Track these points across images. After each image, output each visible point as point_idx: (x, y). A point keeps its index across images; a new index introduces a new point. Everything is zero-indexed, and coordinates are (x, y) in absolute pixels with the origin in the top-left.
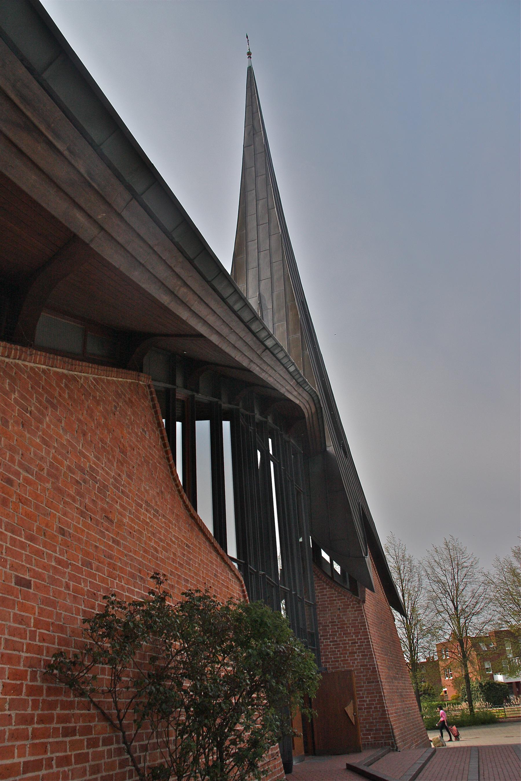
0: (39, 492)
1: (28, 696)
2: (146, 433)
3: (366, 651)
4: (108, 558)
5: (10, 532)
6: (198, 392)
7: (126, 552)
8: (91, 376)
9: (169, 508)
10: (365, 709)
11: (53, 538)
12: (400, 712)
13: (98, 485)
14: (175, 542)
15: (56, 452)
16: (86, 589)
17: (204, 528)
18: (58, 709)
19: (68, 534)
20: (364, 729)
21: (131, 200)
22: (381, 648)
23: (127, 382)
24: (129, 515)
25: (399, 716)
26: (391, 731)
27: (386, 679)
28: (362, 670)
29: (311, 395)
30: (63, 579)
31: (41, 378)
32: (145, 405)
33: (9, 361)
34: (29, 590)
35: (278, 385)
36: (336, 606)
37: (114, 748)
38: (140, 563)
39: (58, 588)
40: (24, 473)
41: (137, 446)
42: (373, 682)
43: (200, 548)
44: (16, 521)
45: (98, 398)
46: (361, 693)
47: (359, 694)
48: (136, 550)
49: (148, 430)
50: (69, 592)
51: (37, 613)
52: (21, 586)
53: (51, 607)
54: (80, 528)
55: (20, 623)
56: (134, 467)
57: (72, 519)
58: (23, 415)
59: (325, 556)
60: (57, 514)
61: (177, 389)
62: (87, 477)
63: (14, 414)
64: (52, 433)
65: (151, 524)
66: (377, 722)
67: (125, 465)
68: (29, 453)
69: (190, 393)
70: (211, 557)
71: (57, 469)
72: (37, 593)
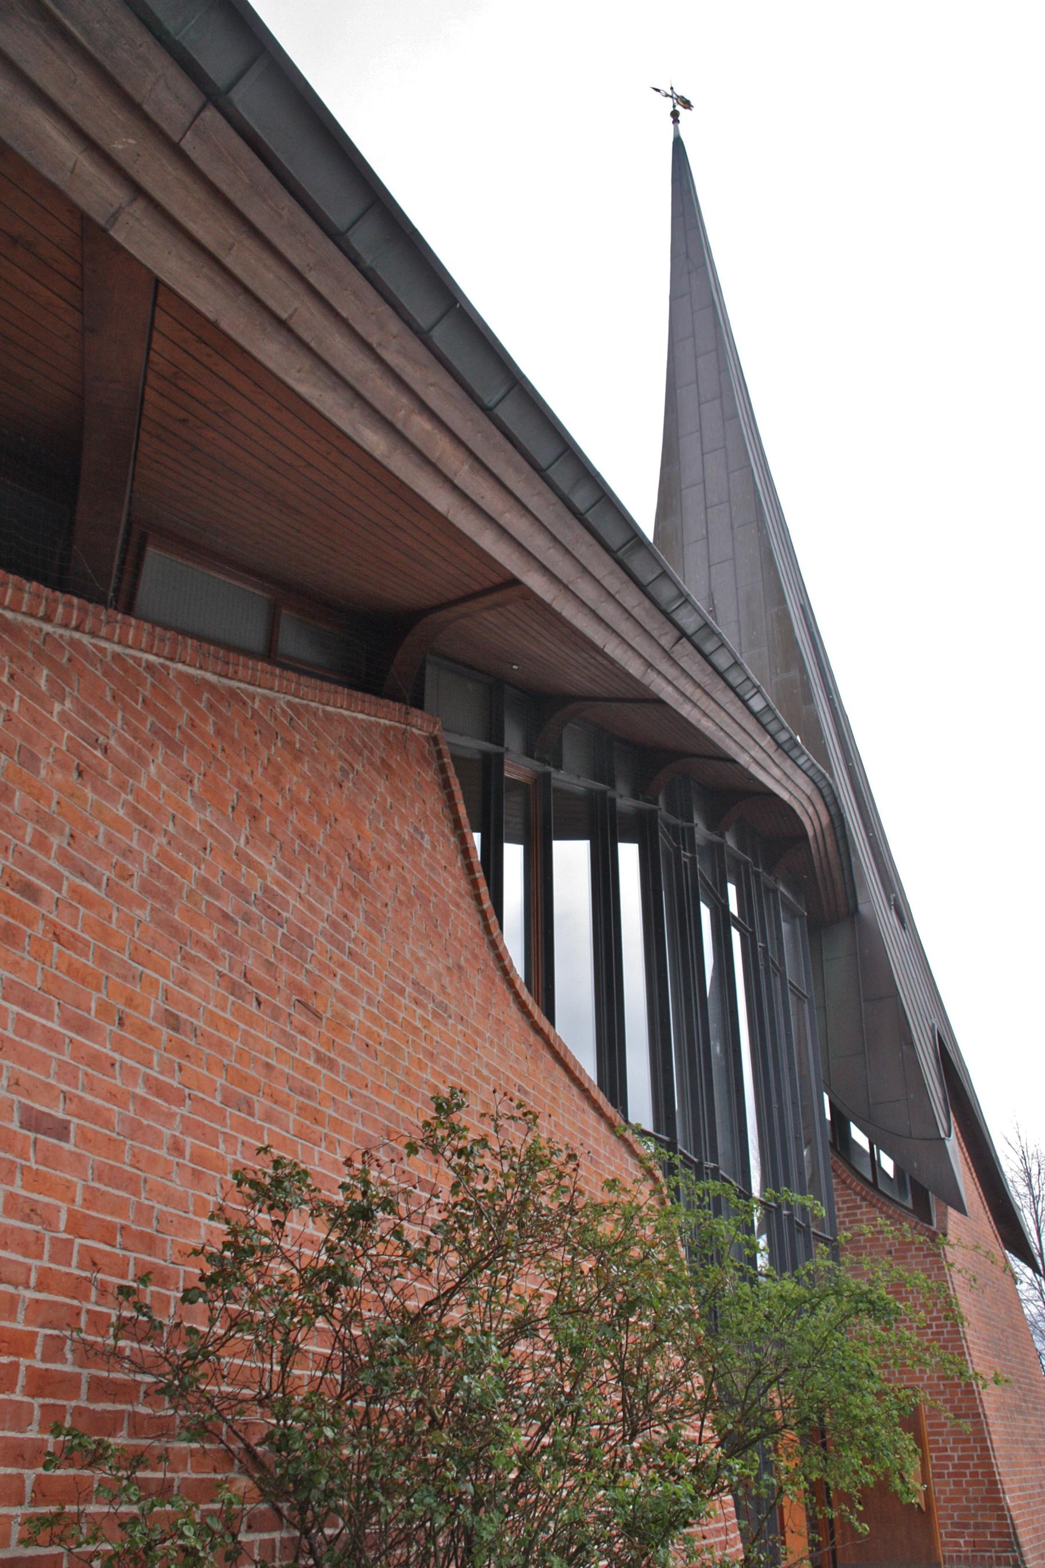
0: (113, 926)
1: (33, 1396)
2: (422, 838)
3: (950, 1345)
4: (302, 1094)
5: (18, 1005)
6: (559, 766)
7: (350, 1086)
8: (283, 699)
9: (477, 1004)
10: (950, 1475)
11: (145, 1031)
12: (1033, 1487)
13: (285, 931)
14: (490, 1079)
15: (169, 843)
16: (230, 1158)
17: (565, 1055)
18: (124, 1433)
19: (188, 1028)
20: (949, 1522)
21: (202, 109)
22: (984, 1339)
23: (379, 724)
24: (367, 1007)
25: (1031, 1496)
26: (1011, 1530)
27: (997, 1410)
28: (942, 1387)
29: (815, 783)
30: (164, 1130)
31: (141, 682)
32: (424, 779)
33: (54, 632)
34: (63, 1144)
35: (727, 740)
36: (883, 1246)
37: (282, 1539)
38: (391, 1115)
39: (148, 1148)
40: (70, 878)
41: (396, 861)
42: (966, 1416)
43: (555, 1099)
44: (39, 984)
45: (297, 746)
46: (940, 1439)
47: (937, 1442)
48: (380, 1086)
49: (430, 833)
50: (181, 1161)
51: (79, 1199)
52: (37, 1131)
53: (125, 1189)
54: (225, 1020)
55: (27, 1219)
56: (386, 905)
57: (205, 997)
58: (83, 752)
59: (858, 1136)
60: (162, 980)
61: (506, 756)
62: (254, 909)
63: (55, 744)
64: (162, 802)
65: (425, 1031)
66: (977, 1508)
67: (363, 897)
68: (92, 836)
69: (537, 766)
70: (584, 1121)
71: (170, 881)
72: (83, 1152)
